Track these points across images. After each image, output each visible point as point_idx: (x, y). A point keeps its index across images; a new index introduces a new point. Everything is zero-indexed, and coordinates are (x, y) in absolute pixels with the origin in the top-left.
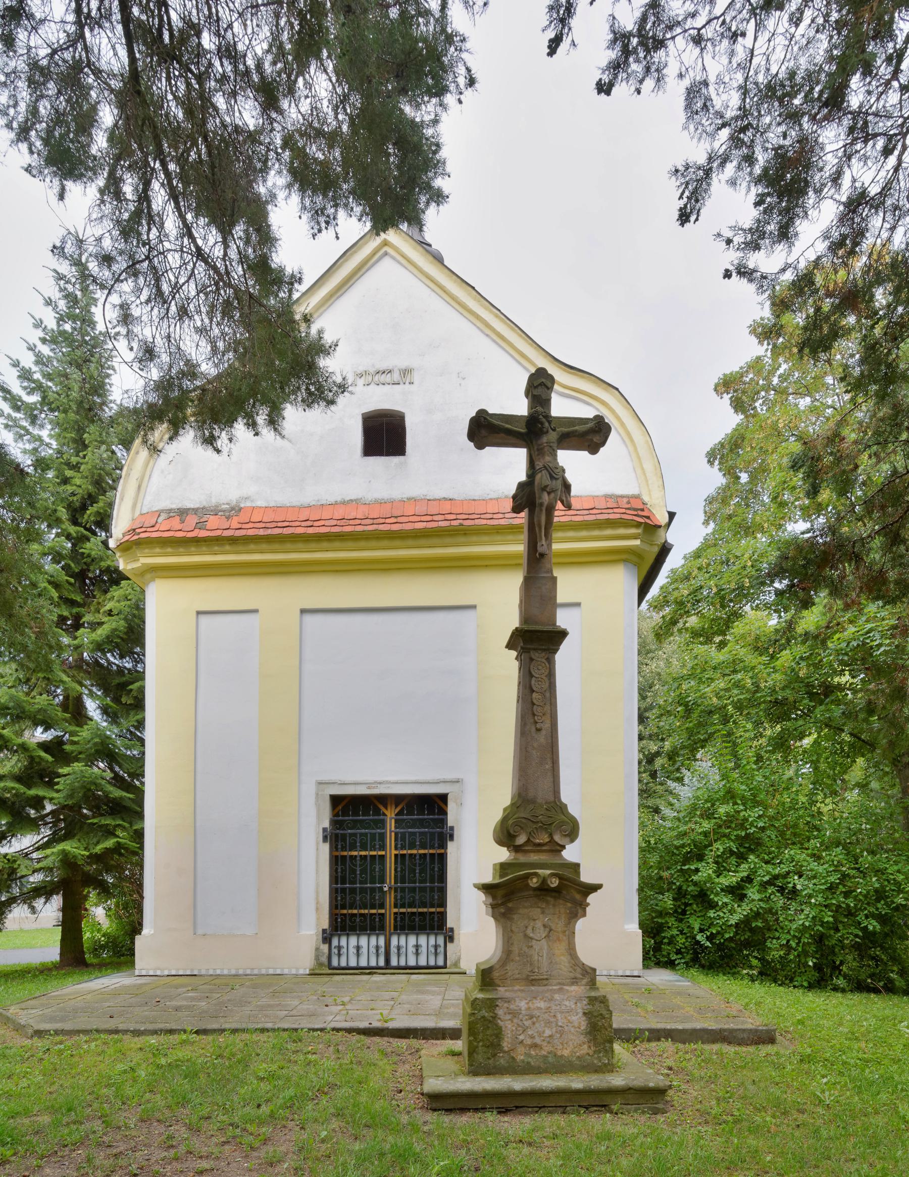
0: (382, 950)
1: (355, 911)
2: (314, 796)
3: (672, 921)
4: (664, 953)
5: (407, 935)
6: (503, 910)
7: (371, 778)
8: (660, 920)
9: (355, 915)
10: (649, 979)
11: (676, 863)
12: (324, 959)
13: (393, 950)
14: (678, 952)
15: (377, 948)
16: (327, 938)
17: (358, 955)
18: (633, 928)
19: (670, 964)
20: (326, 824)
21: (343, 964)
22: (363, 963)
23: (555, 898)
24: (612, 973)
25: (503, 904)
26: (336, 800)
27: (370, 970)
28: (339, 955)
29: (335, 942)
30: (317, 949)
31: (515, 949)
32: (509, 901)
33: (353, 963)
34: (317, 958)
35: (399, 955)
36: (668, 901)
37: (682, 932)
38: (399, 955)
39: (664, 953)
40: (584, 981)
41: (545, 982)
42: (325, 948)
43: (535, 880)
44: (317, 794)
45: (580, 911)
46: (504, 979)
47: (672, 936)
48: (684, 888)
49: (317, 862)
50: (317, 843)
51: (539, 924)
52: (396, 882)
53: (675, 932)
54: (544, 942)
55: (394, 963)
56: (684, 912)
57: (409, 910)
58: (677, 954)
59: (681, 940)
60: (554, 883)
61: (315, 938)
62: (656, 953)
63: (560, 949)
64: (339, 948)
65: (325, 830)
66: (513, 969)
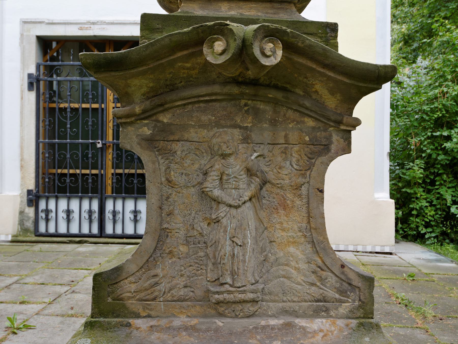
0: (96, 216)
1: (65, 171)
2: (18, 36)
3: (420, 191)
4: (413, 226)
5: (124, 199)
6: (147, 131)
7: (83, 18)
8: (409, 191)
9: (65, 175)
10: (403, 256)
11: (425, 129)
12: (30, 224)
13: (108, 216)
14: (427, 225)
15: (90, 212)
16: (33, 199)
17: (69, 220)
18: (383, 197)
19: (419, 238)
20: (32, 70)
21: (52, 230)
22: (74, 230)
23: (275, 102)
24: (360, 248)
25: (146, 115)
26: (44, 43)
27: (80, 238)
28: (47, 220)
29: (42, 205)
30: (21, 213)
31: (178, 225)
32: (162, 107)
33: (63, 229)
34: (21, 222)
35: (115, 222)
36: (417, 170)
37: (431, 203)
38: (115, 222)
39: (413, 226)
40: (344, 308)
41: (251, 308)
42: (30, 212)
43: (219, 46)
44: (22, 35)
45: (335, 138)
46: (149, 298)
47: (421, 208)
48: (434, 156)
49: (22, 113)
50: (22, 92)
51: (235, 166)
52: (113, 140)
53: (425, 204)
54: (247, 211)
55: (109, 230)
56: (433, 183)
57: (127, 171)
58: (426, 227)
59: (430, 212)
60: (272, 55)
61: (19, 200)
62: (408, 229)
63: (288, 226)
64: (47, 211)
65: (30, 76)
66: (171, 274)
